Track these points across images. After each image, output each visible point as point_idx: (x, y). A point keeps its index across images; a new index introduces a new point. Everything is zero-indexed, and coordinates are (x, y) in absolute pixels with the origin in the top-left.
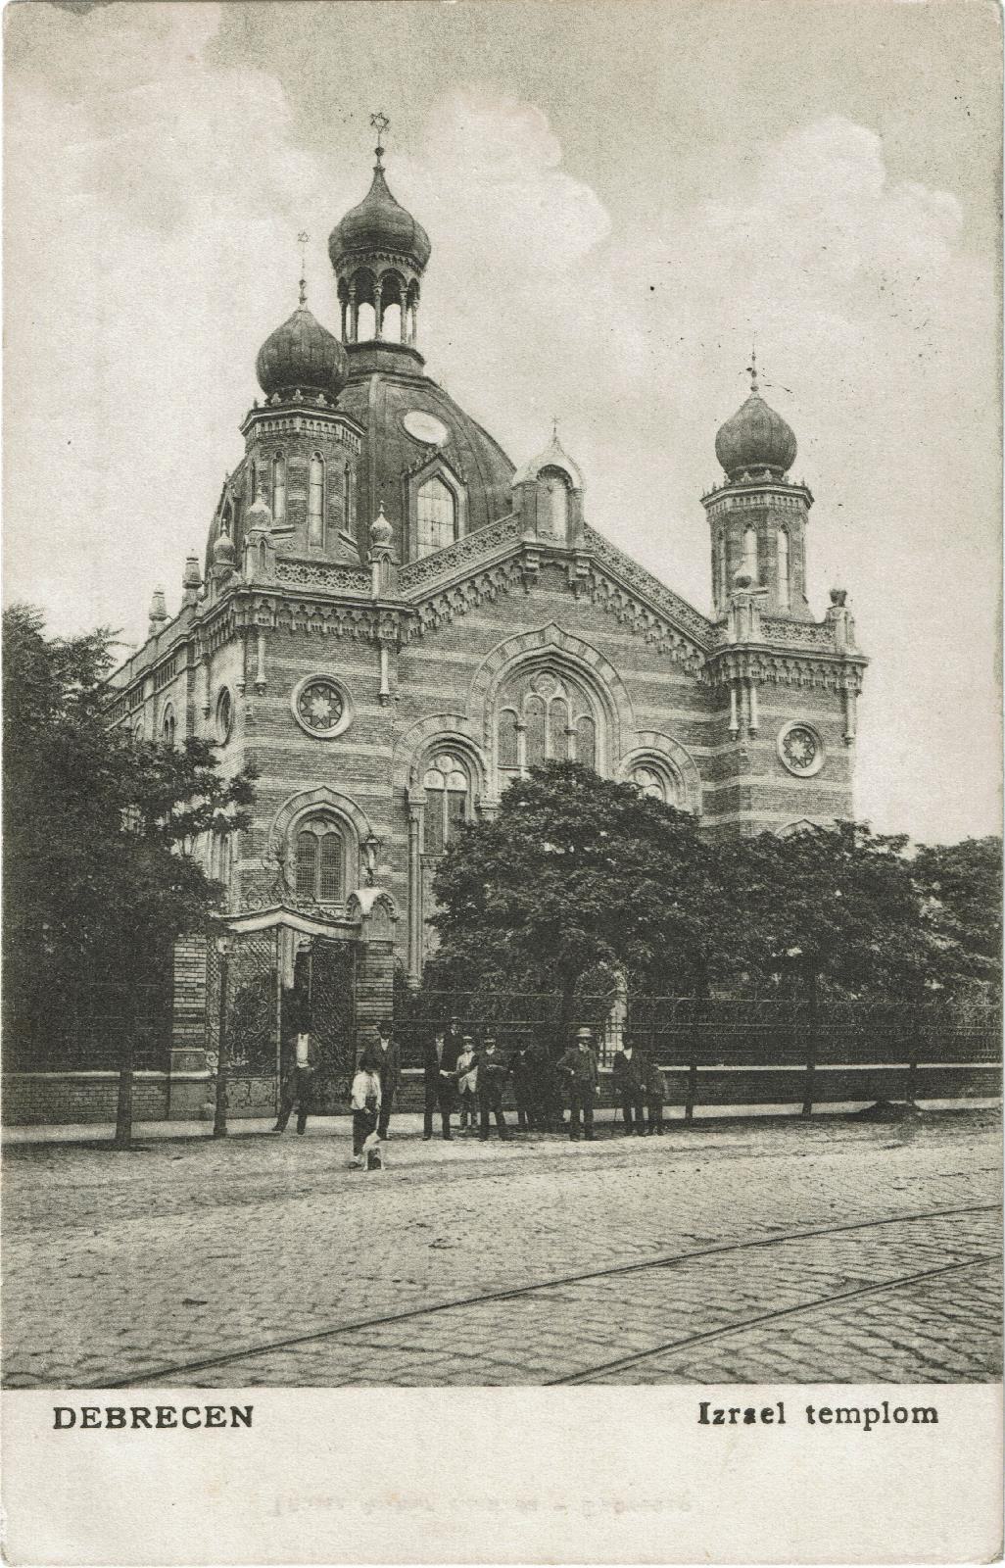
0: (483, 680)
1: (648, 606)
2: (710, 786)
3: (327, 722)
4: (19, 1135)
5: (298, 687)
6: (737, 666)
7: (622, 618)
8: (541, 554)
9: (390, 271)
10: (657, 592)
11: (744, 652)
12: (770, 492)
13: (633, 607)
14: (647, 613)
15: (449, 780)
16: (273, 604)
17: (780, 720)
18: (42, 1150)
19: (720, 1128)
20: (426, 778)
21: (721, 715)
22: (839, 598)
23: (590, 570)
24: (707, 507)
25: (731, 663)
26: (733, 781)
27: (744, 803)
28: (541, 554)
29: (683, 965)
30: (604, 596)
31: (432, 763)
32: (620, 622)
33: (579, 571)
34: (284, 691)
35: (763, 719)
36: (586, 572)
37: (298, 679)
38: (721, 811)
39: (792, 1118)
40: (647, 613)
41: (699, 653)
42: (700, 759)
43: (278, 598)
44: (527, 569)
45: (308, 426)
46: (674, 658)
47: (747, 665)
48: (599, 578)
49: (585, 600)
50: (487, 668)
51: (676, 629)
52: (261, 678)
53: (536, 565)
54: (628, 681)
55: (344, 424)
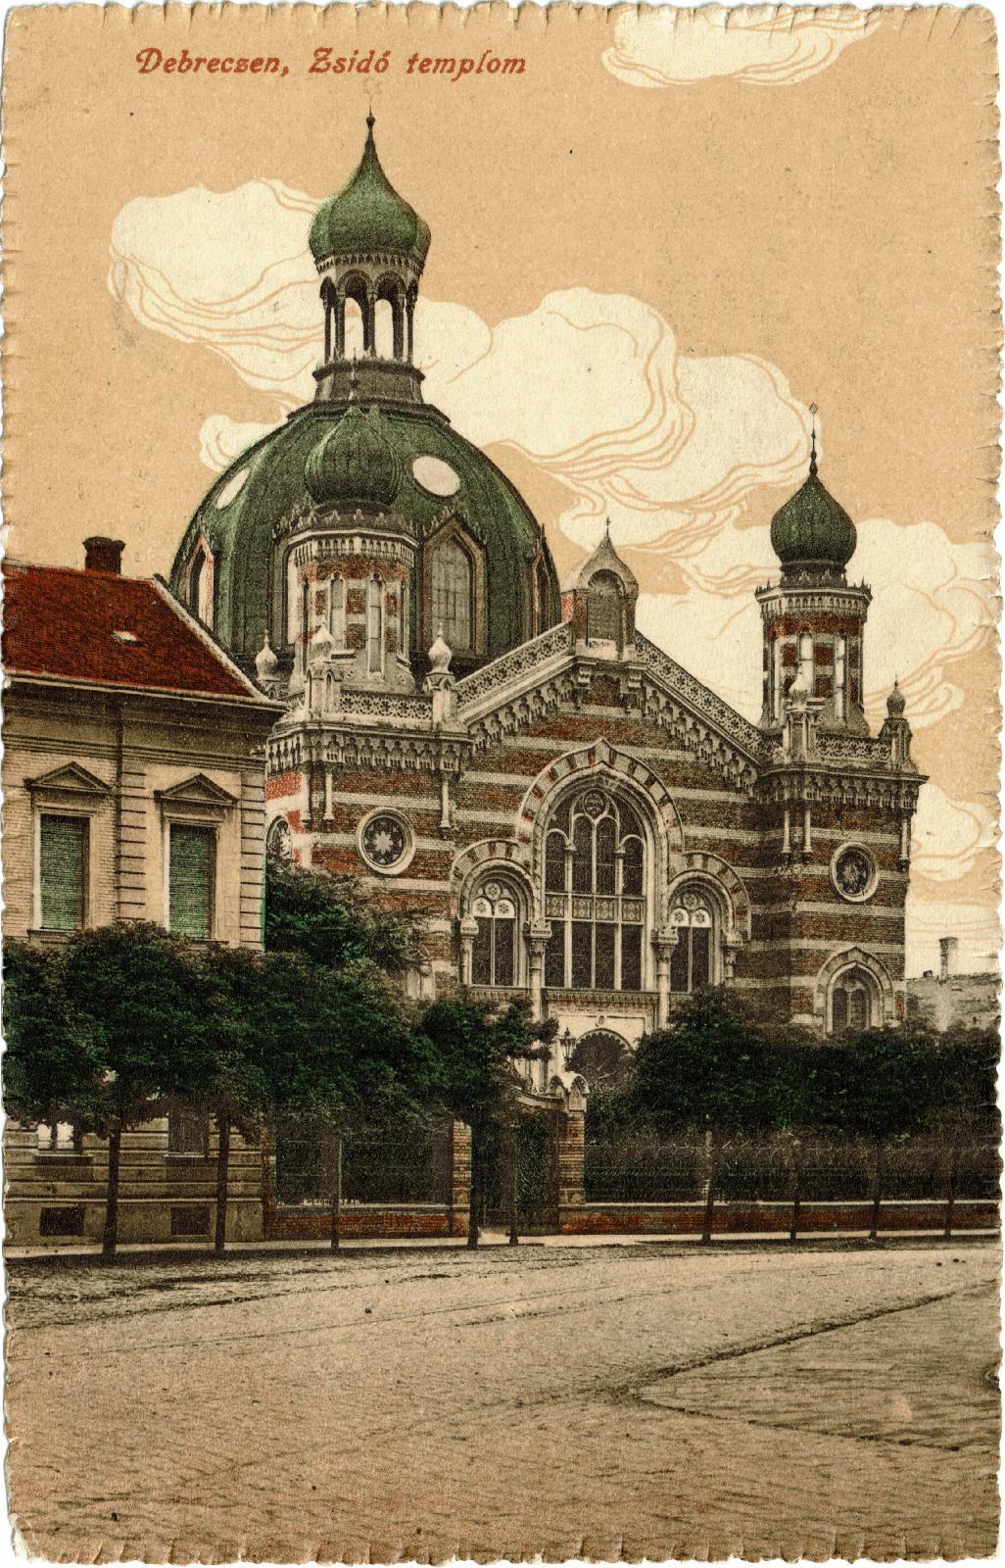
0: (528, 801)
1: (698, 719)
2: (759, 910)
3: (389, 857)
4: (18, 1253)
5: (363, 822)
6: (791, 786)
7: (673, 733)
8: (593, 668)
9: (351, 272)
10: (722, 713)
11: (799, 772)
12: (829, 594)
13: (684, 720)
14: (699, 727)
15: (497, 909)
16: (341, 741)
17: (834, 844)
18: (51, 1265)
19: (945, 1245)
20: (474, 907)
21: (773, 835)
22: (896, 705)
23: (641, 682)
24: (761, 601)
25: (785, 783)
26: (786, 908)
27: (793, 931)
28: (593, 668)
29: (811, 1113)
30: (709, 751)
31: (481, 892)
32: (670, 737)
33: (630, 685)
34: (350, 827)
35: (816, 843)
36: (638, 685)
37: (364, 813)
38: (772, 936)
39: (938, 1239)
40: (712, 737)
41: (751, 769)
42: (748, 882)
43: (345, 734)
44: (580, 684)
45: (368, 546)
46: (725, 774)
47: (801, 785)
48: (649, 690)
49: (635, 714)
50: (538, 793)
51: (715, 733)
52: (329, 815)
53: (588, 681)
54: (678, 800)
55: (403, 542)
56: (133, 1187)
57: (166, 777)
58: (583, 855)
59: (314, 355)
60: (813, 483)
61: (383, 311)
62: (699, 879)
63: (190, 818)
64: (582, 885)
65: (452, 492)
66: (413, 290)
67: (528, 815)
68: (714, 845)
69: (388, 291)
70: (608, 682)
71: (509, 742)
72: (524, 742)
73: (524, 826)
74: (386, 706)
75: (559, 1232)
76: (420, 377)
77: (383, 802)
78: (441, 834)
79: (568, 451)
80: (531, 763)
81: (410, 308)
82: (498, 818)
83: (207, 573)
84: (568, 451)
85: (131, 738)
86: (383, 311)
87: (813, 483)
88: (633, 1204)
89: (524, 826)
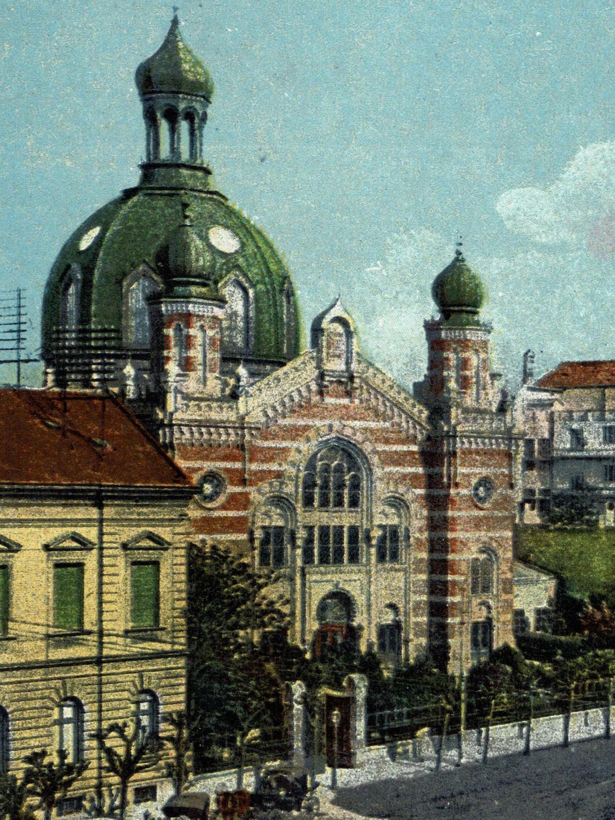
21: (436, 470)
57: (128, 533)
59: (140, 154)
60: (459, 259)
61: (184, 126)
62: (394, 497)
63: (143, 556)
64: (324, 503)
65: (233, 251)
66: (204, 118)
67: (293, 464)
68: (404, 477)
71: (281, 422)
72: (287, 422)
76: (207, 172)
80: (294, 433)
81: (201, 128)
82: (274, 467)
85: (109, 512)
86: (184, 126)
87: (459, 259)
88: (316, 551)
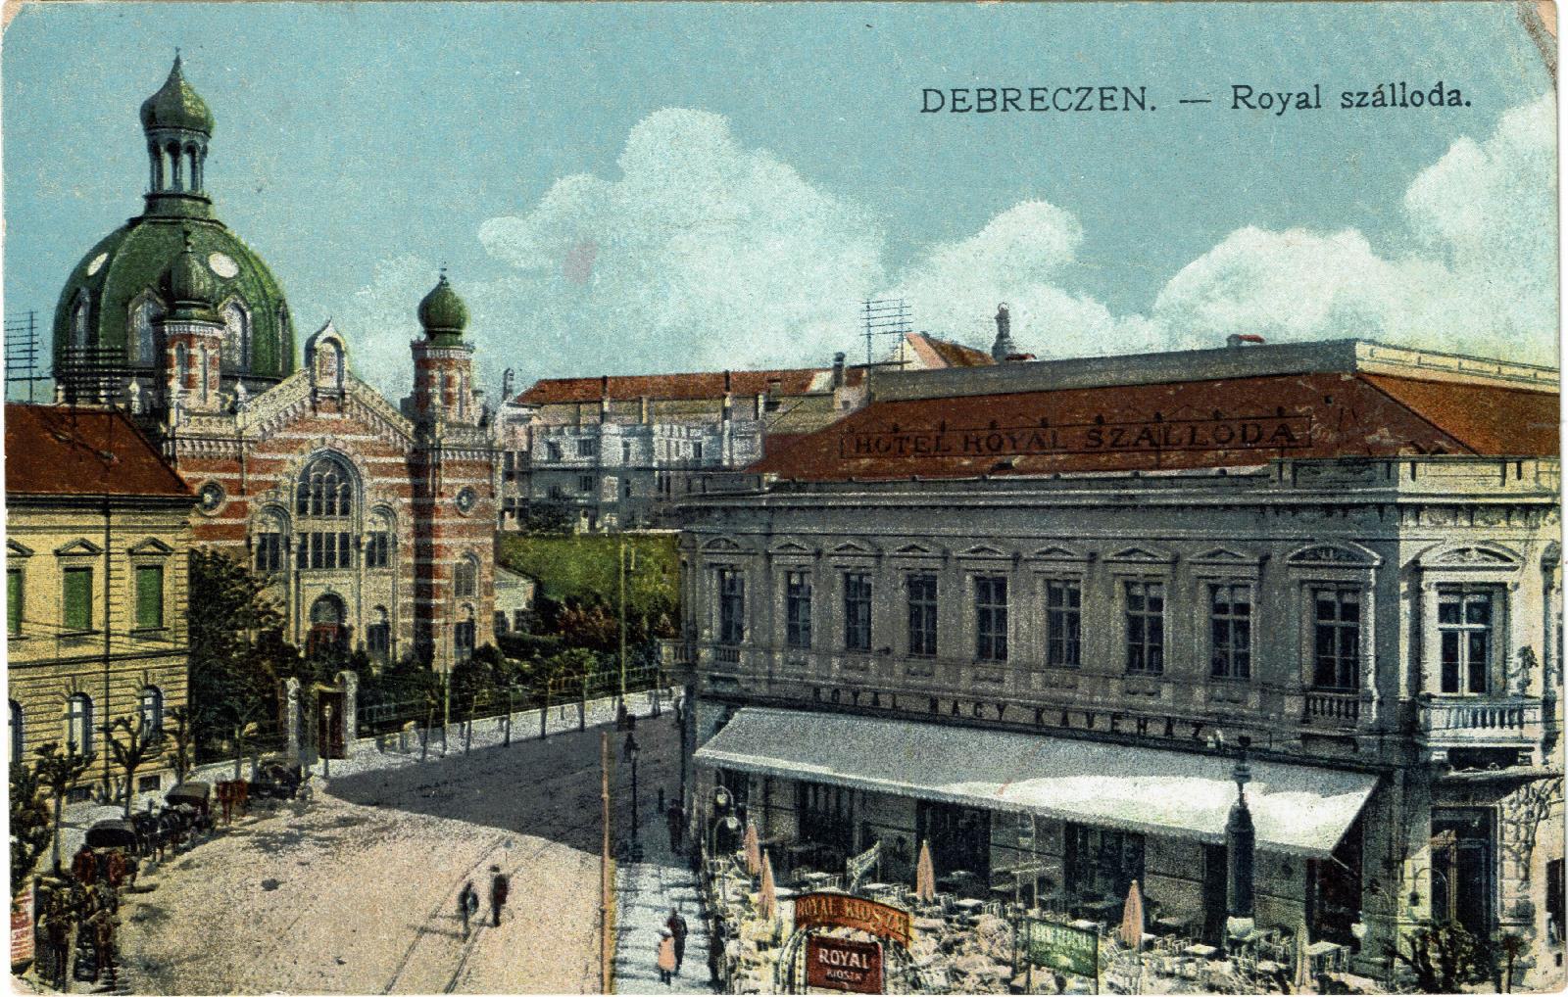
3: (211, 507)
21: (422, 481)
50: (293, 463)
56: (117, 692)
58: (318, 495)
59: (145, 184)
61: (186, 159)
64: (317, 511)
67: (288, 475)
68: (392, 487)
69: (191, 150)
70: (339, 399)
71: (277, 435)
73: (287, 481)
74: (210, 421)
75: (804, 787)
77: (208, 476)
78: (241, 492)
79: (1435, 353)
80: (290, 446)
81: (201, 161)
82: (271, 478)
83: (1231, 470)
84: (1435, 353)
86: (186, 159)
89: (287, 481)
